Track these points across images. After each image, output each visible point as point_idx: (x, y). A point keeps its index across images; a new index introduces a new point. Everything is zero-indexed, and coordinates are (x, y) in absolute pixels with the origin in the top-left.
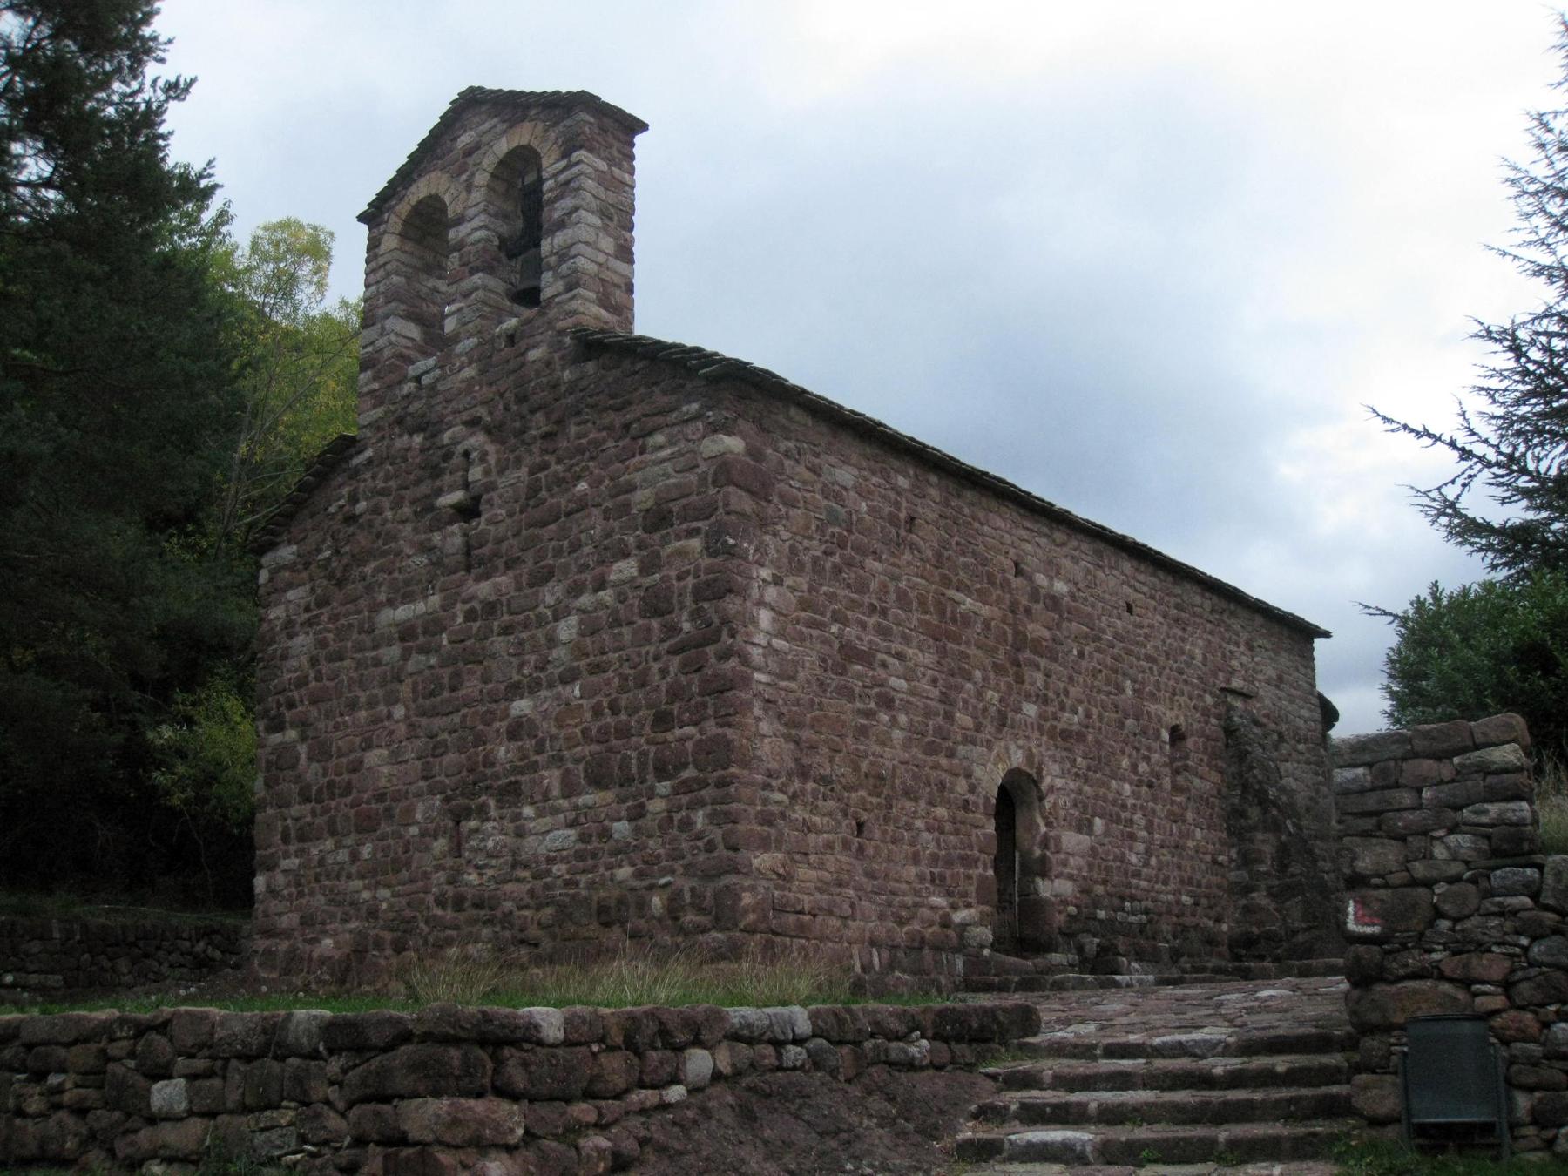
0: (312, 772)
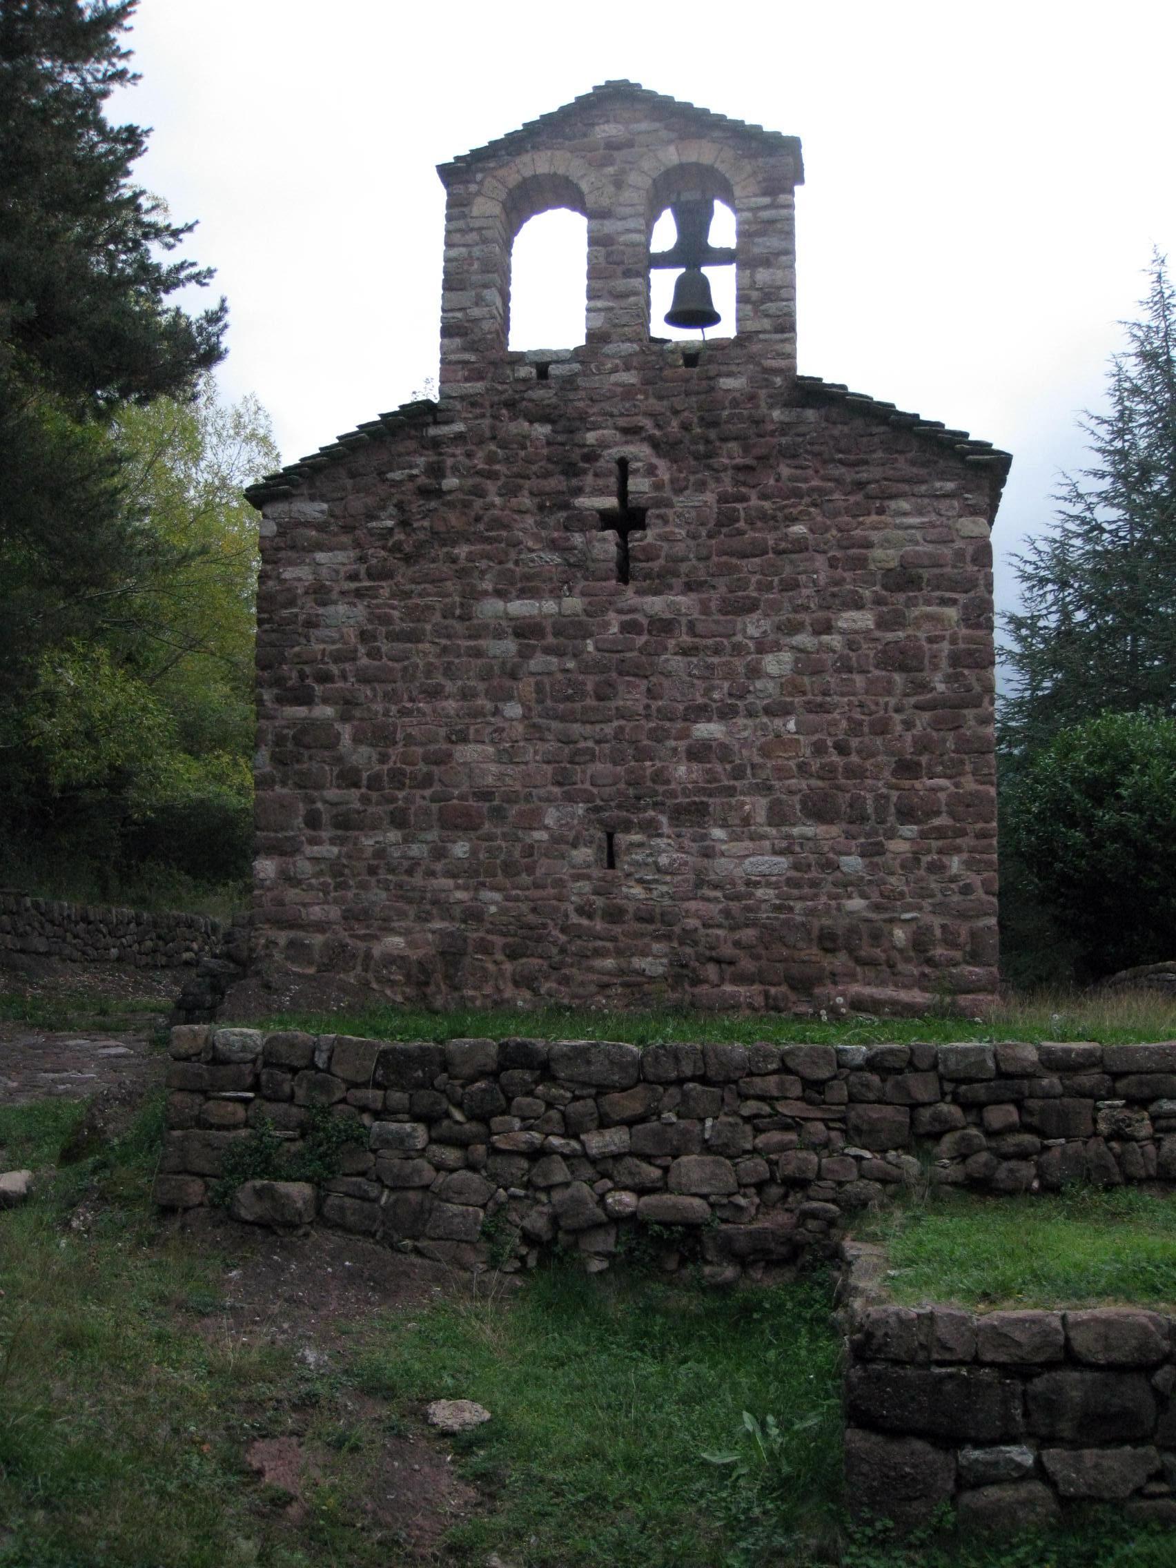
0: (362, 756)
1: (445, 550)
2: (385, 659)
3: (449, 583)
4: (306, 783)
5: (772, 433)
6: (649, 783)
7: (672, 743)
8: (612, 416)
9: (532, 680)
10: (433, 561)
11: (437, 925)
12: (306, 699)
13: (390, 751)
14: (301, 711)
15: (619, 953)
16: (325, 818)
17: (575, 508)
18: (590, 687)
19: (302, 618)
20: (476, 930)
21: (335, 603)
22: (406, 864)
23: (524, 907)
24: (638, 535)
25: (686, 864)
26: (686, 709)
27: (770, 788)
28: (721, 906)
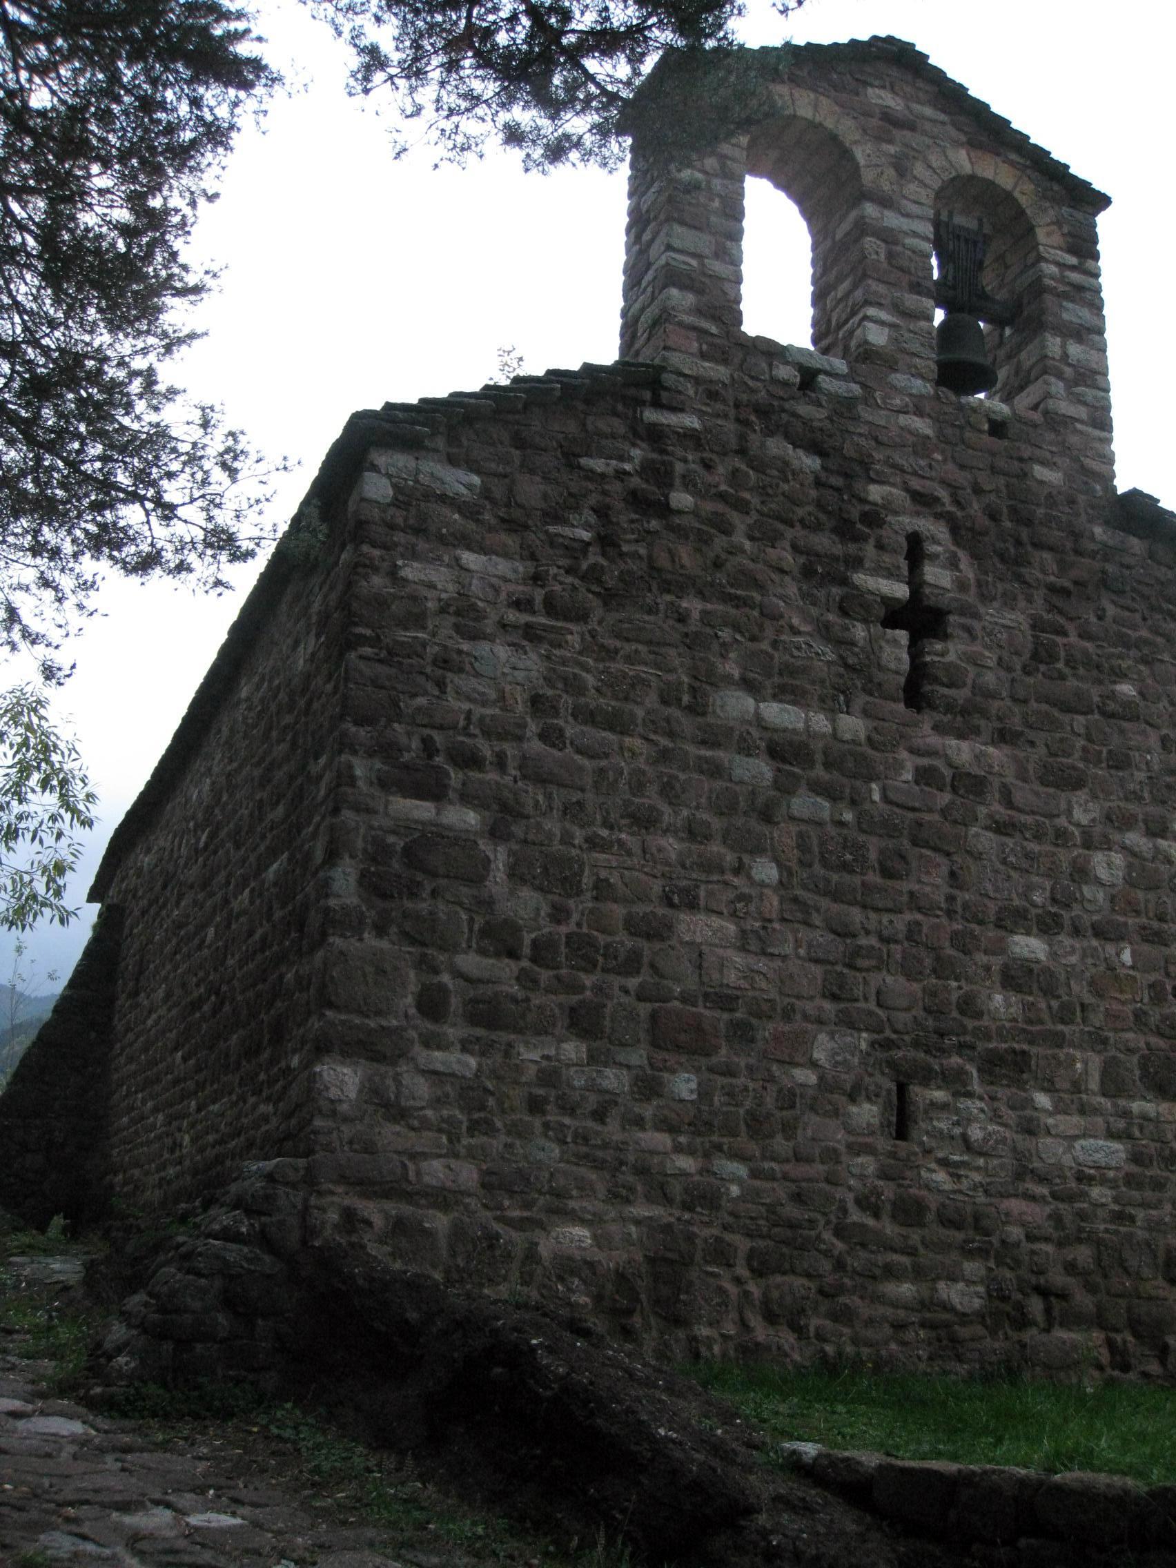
0: (525, 906)
1: (669, 598)
2: (569, 750)
3: (672, 652)
4: (425, 937)
5: (1093, 554)
6: (955, 1014)
7: (981, 958)
8: (903, 471)
9: (794, 829)
10: (649, 612)
11: (641, 1210)
12: (436, 792)
13: (571, 903)
14: (423, 810)
15: (918, 1273)
16: (455, 1002)
17: (856, 588)
18: (873, 855)
19: (432, 650)
20: (708, 1224)
21: (490, 638)
22: (593, 1100)
23: (781, 1191)
24: (939, 647)
25: (1004, 1141)
26: (1001, 910)
27: (1105, 1041)
28: (1048, 1210)
